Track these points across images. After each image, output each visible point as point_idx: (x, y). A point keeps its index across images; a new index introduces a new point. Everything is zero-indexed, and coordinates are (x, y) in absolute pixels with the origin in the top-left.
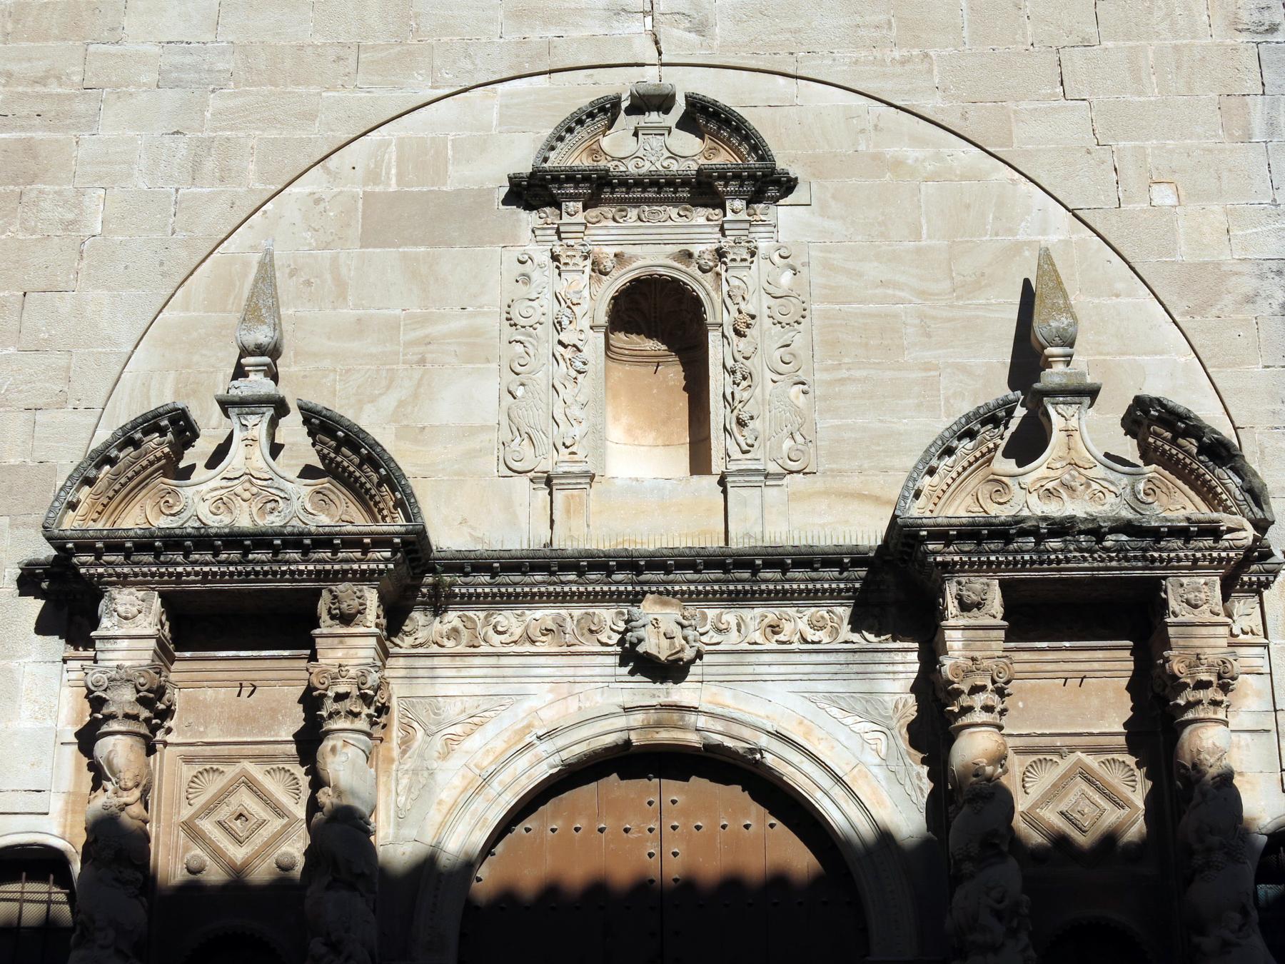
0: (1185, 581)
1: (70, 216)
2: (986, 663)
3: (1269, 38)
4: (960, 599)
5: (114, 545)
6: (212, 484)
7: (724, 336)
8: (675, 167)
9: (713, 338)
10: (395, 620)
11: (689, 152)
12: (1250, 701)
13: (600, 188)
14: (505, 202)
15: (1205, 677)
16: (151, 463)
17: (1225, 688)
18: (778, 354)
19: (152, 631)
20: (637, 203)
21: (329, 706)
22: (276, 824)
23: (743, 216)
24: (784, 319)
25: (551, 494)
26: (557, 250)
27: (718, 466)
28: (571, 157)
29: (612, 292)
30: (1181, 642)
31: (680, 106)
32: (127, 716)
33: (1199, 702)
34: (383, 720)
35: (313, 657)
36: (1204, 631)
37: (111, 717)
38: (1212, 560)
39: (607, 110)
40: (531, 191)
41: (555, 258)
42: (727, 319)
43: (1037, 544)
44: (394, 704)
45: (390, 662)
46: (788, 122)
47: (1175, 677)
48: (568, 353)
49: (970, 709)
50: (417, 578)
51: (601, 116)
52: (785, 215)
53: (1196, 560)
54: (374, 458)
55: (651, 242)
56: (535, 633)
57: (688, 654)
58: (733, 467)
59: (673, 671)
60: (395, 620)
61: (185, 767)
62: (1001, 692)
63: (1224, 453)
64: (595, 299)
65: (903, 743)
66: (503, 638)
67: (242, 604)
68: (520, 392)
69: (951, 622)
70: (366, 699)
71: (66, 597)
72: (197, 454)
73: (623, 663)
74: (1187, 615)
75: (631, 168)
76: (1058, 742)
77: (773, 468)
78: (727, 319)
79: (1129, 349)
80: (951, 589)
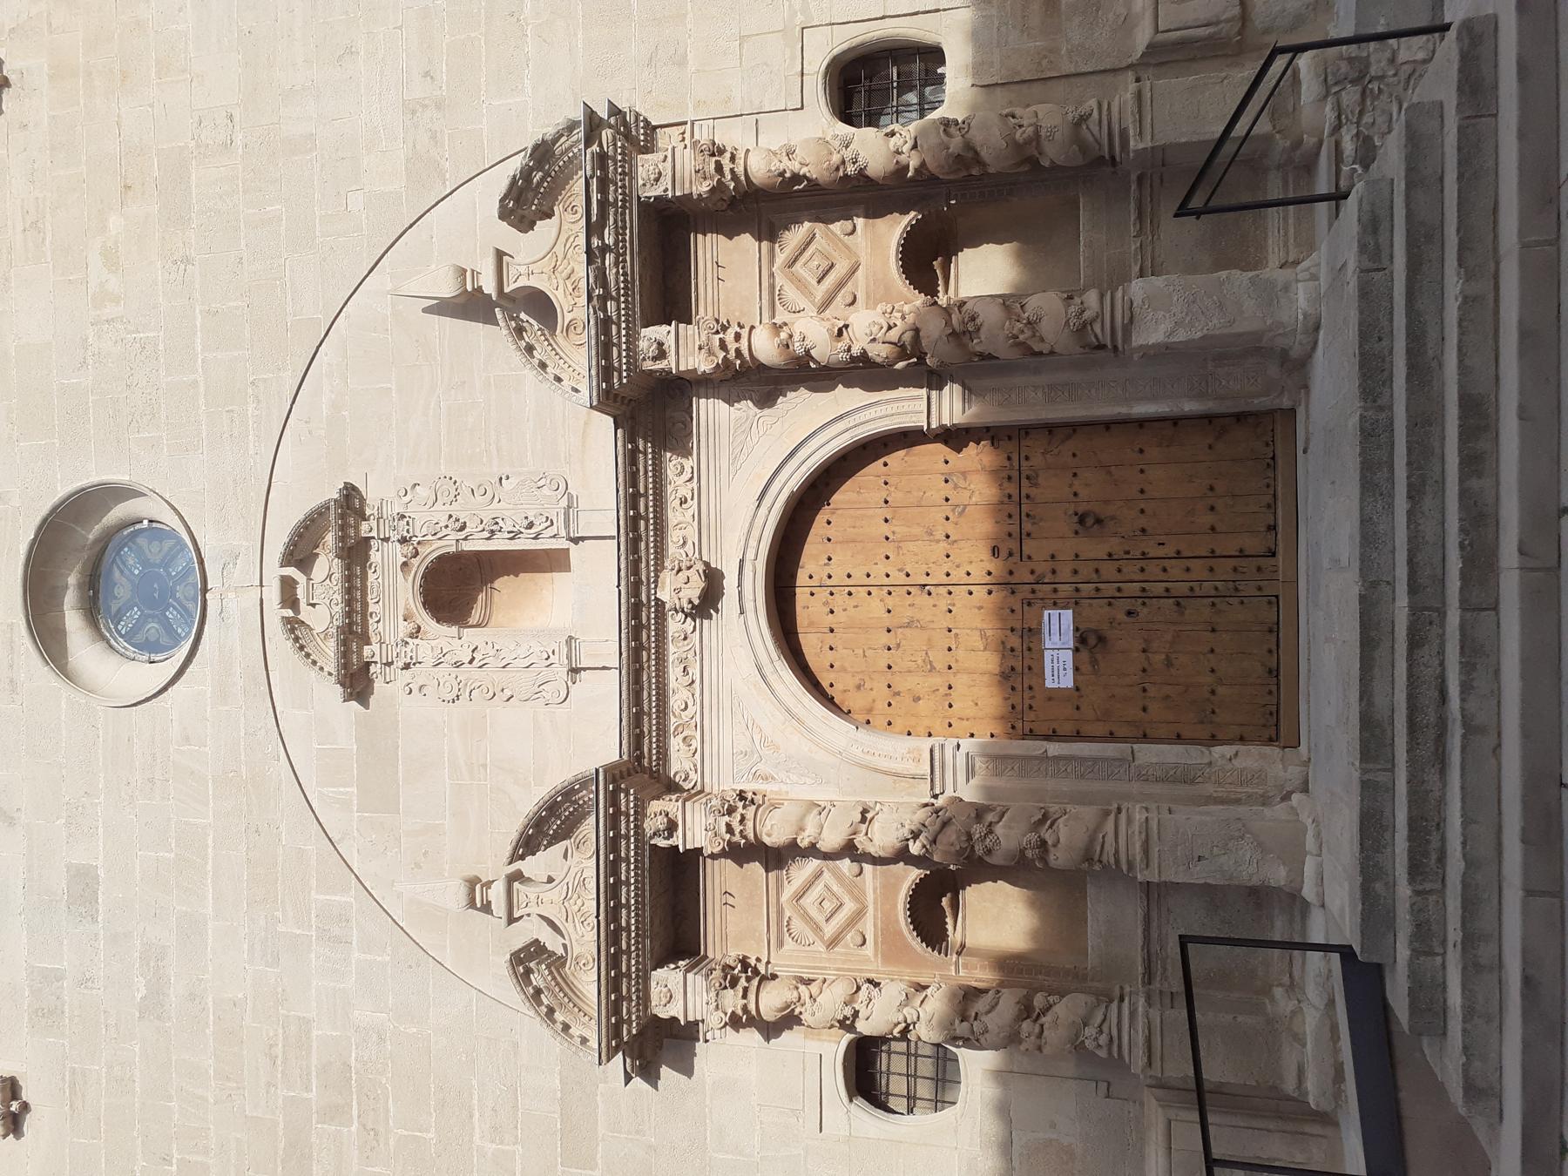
0: (641, 182)
1: (375, 1037)
2: (704, 338)
3: (236, 119)
4: (655, 359)
5: (615, 1009)
6: (571, 930)
7: (465, 539)
8: (337, 576)
9: (467, 546)
10: (672, 787)
11: (327, 564)
12: (733, 136)
13: (353, 631)
14: (367, 708)
15: (713, 166)
16: (554, 978)
17: (721, 152)
18: (479, 498)
19: (679, 975)
20: (365, 605)
21: (737, 838)
22: (826, 875)
23: (374, 524)
24: (453, 493)
25: (585, 669)
26: (401, 664)
27: (562, 544)
28: (328, 652)
29: (433, 623)
30: (687, 185)
31: (291, 571)
32: (745, 996)
33: (732, 170)
34: (749, 795)
35: (699, 851)
36: (678, 167)
37: (745, 1009)
38: (623, 160)
39: (293, 626)
40: (356, 682)
41: (407, 667)
42: (455, 536)
43: (612, 298)
44: (739, 787)
45: (707, 790)
46: (304, 491)
47: (713, 190)
48: (478, 656)
49: (738, 351)
50: (642, 771)
51: (298, 633)
52: (373, 495)
53: (623, 173)
54: (552, 807)
55: (394, 591)
56: (688, 680)
57: (701, 567)
58: (563, 533)
59: (713, 578)
60: (672, 787)
61: (786, 947)
62: (725, 328)
63: (541, 149)
64: (440, 635)
65: (767, 411)
66: (690, 704)
67: (663, 906)
68: (508, 693)
69: (673, 366)
70: (731, 811)
71: (655, 1046)
72: (552, 943)
73: (710, 617)
74: (666, 182)
75: (338, 609)
76: (765, 284)
77: (564, 502)
78: (455, 536)
79: (470, 234)
80: (649, 365)
